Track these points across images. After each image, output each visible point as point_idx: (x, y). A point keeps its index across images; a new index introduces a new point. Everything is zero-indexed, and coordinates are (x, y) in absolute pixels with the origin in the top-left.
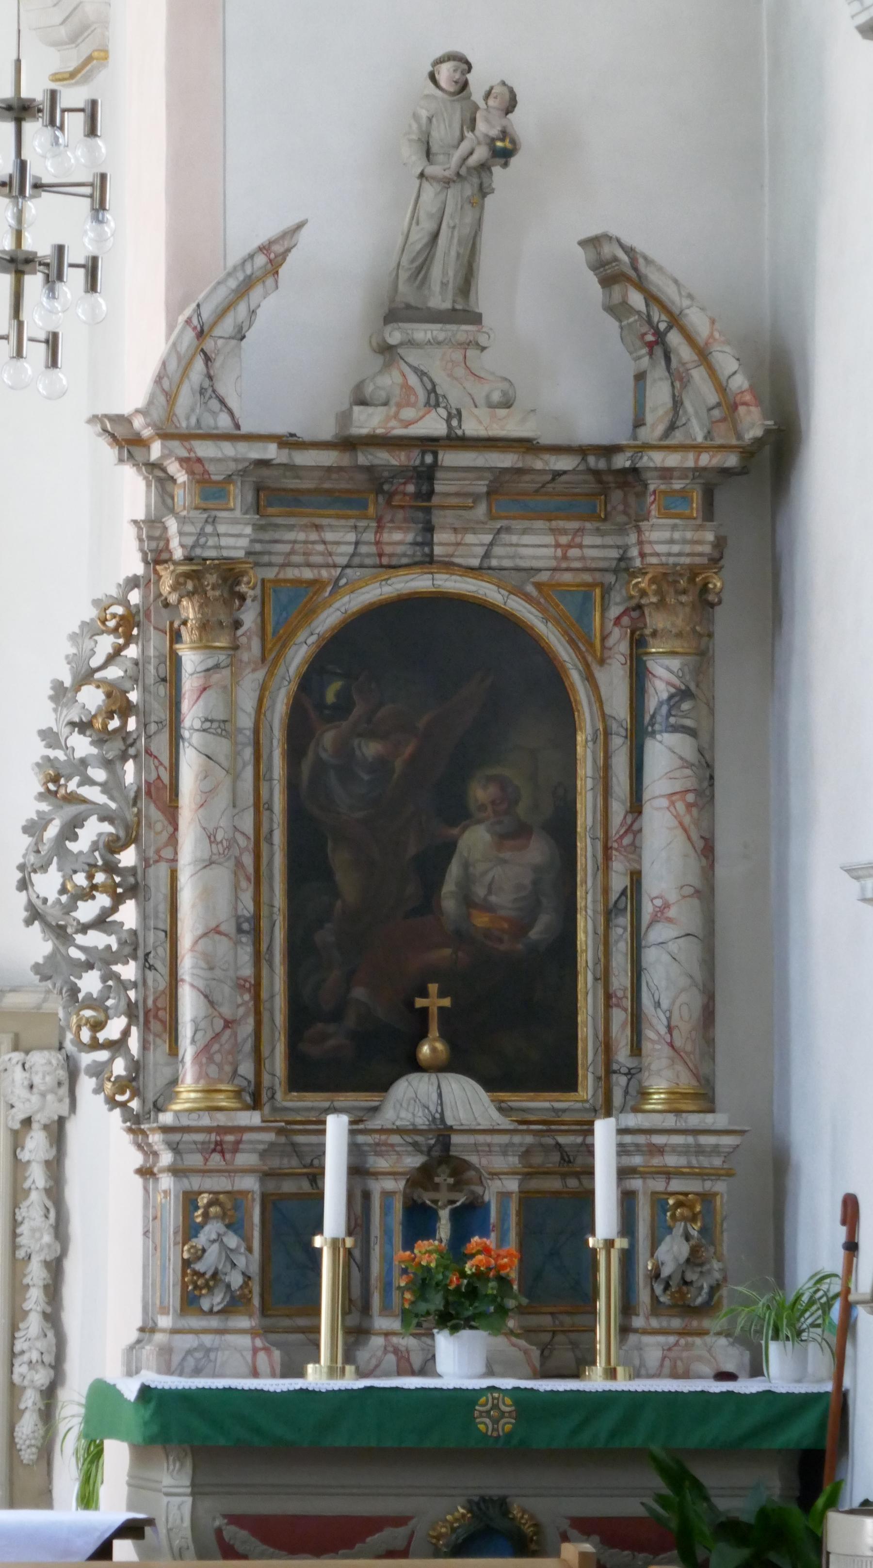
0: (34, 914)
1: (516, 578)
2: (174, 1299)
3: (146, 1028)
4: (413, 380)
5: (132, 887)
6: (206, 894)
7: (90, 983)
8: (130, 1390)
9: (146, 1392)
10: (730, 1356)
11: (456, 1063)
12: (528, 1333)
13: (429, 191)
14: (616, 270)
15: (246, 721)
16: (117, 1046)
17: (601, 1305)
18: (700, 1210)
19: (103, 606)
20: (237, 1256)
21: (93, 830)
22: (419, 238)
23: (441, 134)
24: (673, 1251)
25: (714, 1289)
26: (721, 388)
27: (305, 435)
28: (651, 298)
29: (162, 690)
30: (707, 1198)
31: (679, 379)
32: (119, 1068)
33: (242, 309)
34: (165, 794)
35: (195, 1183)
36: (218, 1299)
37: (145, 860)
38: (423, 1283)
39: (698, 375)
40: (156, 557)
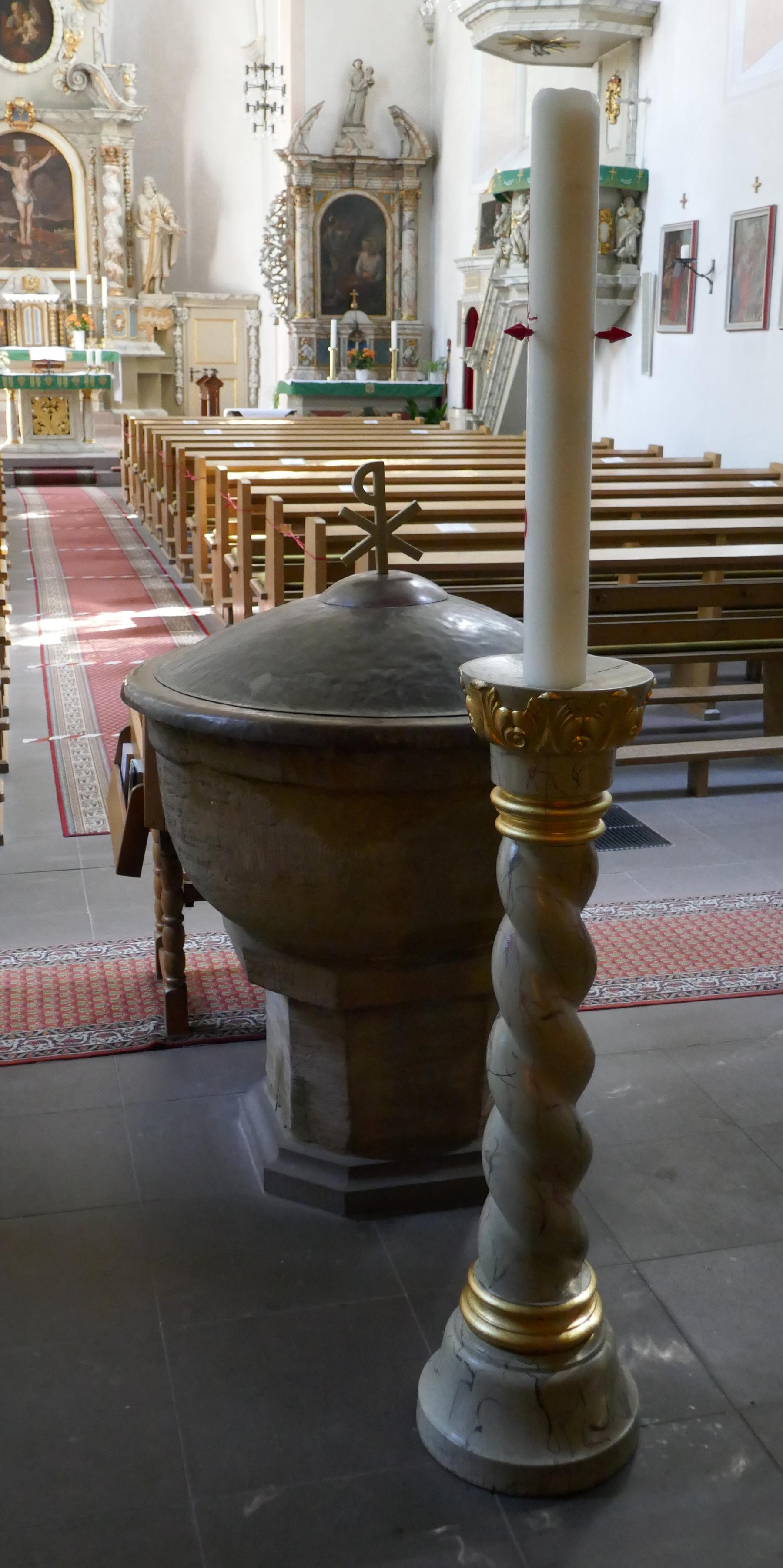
0: (263, 272)
1: (372, 191)
2: (297, 362)
3: (289, 300)
4: (350, 142)
5: (285, 265)
6: (303, 267)
7: (276, 288)
8: (289, 382)
9: (293, 383)
10: (420, 376)
11: (360, 308)
12: (376, 371)
13: (353, 94)
14: (397, 115)
15: (311, 225)
16: (283, 304)
17: (393, 365)
18: (414, 343)
19: (277, 197)
20: (311, 352)
21: (277, 251)
22: (351, 105)
23: (356, 79)
24: (408, 352)
25: (417, 361)
26: (422, 145)
27: (324, 155)
28: (406, 122)
29: (291, 218)
30: (416, 340)
31: (412, 142)
32: (283, 309)
33: (310, 123)
34: (292, 243)
35: (301, 335)
36: (306, 362)
37: (288, 260)
38: (354, 358)
39: (416, 141)
40: (290, 184)
